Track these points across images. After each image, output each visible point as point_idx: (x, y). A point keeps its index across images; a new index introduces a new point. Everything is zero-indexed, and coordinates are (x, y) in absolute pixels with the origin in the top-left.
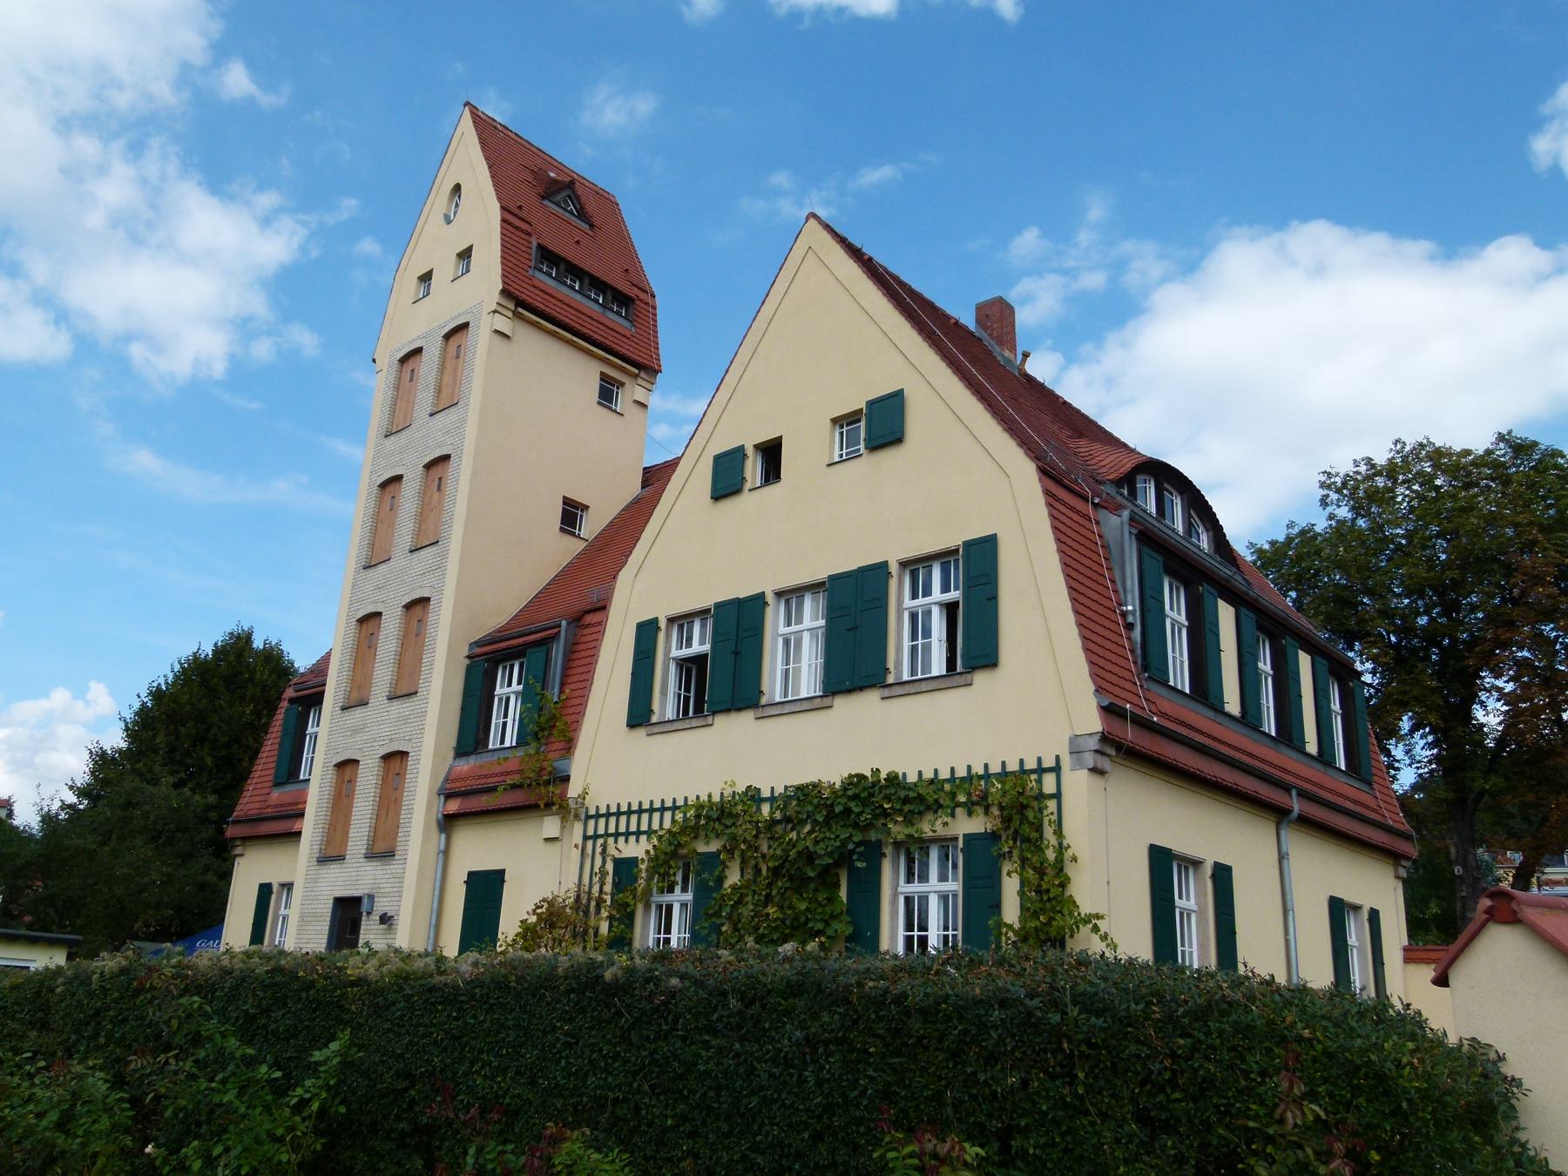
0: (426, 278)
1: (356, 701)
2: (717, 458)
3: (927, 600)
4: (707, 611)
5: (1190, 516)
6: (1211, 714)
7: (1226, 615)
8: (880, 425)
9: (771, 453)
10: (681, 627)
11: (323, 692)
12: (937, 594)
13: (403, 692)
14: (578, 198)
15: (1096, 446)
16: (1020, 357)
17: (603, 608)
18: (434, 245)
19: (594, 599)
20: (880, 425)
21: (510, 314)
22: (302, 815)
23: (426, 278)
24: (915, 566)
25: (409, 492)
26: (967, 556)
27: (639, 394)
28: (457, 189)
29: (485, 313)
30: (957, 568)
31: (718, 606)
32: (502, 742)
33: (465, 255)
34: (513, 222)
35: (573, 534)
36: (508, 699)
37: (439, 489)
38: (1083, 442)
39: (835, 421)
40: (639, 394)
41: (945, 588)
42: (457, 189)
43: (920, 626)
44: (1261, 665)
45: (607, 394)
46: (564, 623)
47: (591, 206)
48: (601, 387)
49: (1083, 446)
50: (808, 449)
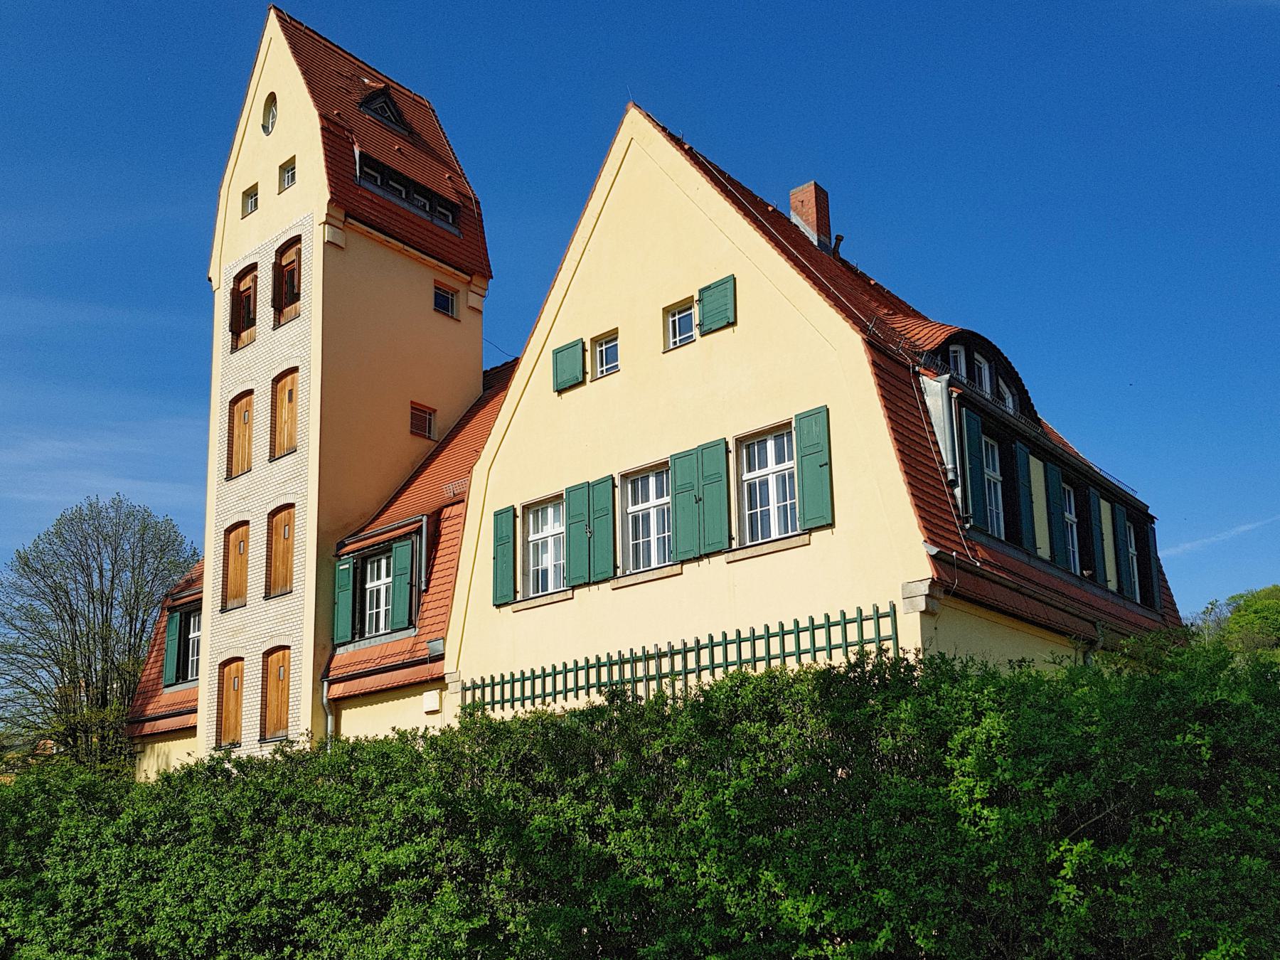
0: (251, 194)
1: (231, 599)
2: (556, 353)
3: (763, 471)
4: (559, 497)
5: (998, 385)
6: (1024, 558)
7: (1036, 468)
8: (701, 315)
9: (608, 340)
10: (634, 483)
11: (201, 599)
12: (653, 501)
13: (276, 587)
14: (395, 104)
15: (910, 321)
16: (833, 242)
17: (460, 500)
18: (252, 156)
19: (449, 491)
20: (701, 315)
21: (341, 226)
22: (195, 711)
23: (251, 194)
24: (636, 478)
25: (261, 403)
26: (799, 428)
27: (474, 300)
28: (272, 99)
29: (316, 225)
30: (790, 441)
31: (569, 490)
32: (377, 630)
33: (288, 169)
34: (335, 139)
35: (424, 437)
36: (378, 591)
37: (290, 400)
38: (900, 317)
39: (667, 311)
40: (474, 300)
41: (660, 495)
42: (272, 99)
43: (640, 522)
44: (1067, 514)
45: (443, 303)
46: (425, 519)
47: (410, 114)
48: (436, 295)
49: (899, 323)
50: (642, 337)
